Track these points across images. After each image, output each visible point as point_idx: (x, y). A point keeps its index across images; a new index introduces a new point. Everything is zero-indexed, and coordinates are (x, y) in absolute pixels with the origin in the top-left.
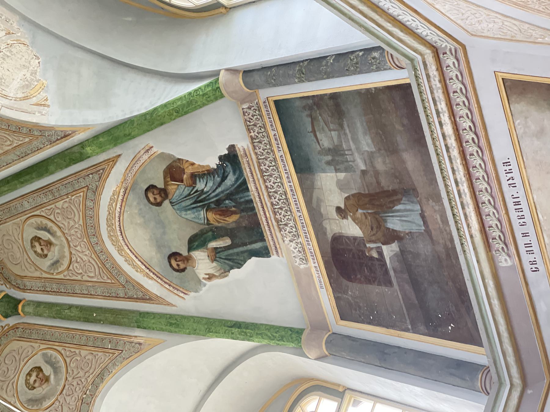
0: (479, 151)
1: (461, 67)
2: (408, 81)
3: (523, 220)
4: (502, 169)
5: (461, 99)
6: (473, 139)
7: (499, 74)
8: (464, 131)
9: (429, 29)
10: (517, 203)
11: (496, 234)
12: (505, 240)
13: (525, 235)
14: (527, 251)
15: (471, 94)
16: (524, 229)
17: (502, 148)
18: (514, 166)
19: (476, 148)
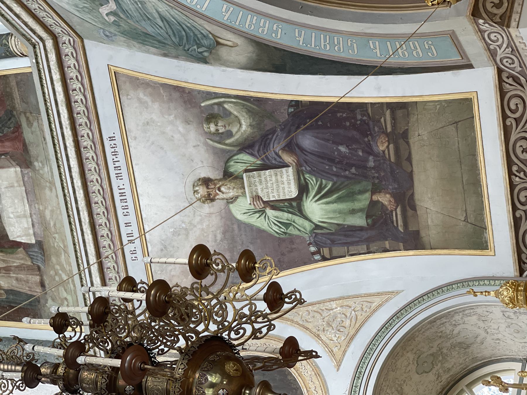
0: (106, 212)
1: (109, 216)
2: (29, 70)
3: (126, 204)
4: (107, 143)
5: (90, 154)
6: (88, 134)
7: (112, 67)
8: (64, 45)
9: (53, 18)
10: (122, 194)
11: (99, 199)
12: (97, 160)
13: (127, 225)
14: (121, 200)
15: (86, 81)
16: (127, 219)
17: (110, 126)
18: (118, 141)
19: (90, 143)
